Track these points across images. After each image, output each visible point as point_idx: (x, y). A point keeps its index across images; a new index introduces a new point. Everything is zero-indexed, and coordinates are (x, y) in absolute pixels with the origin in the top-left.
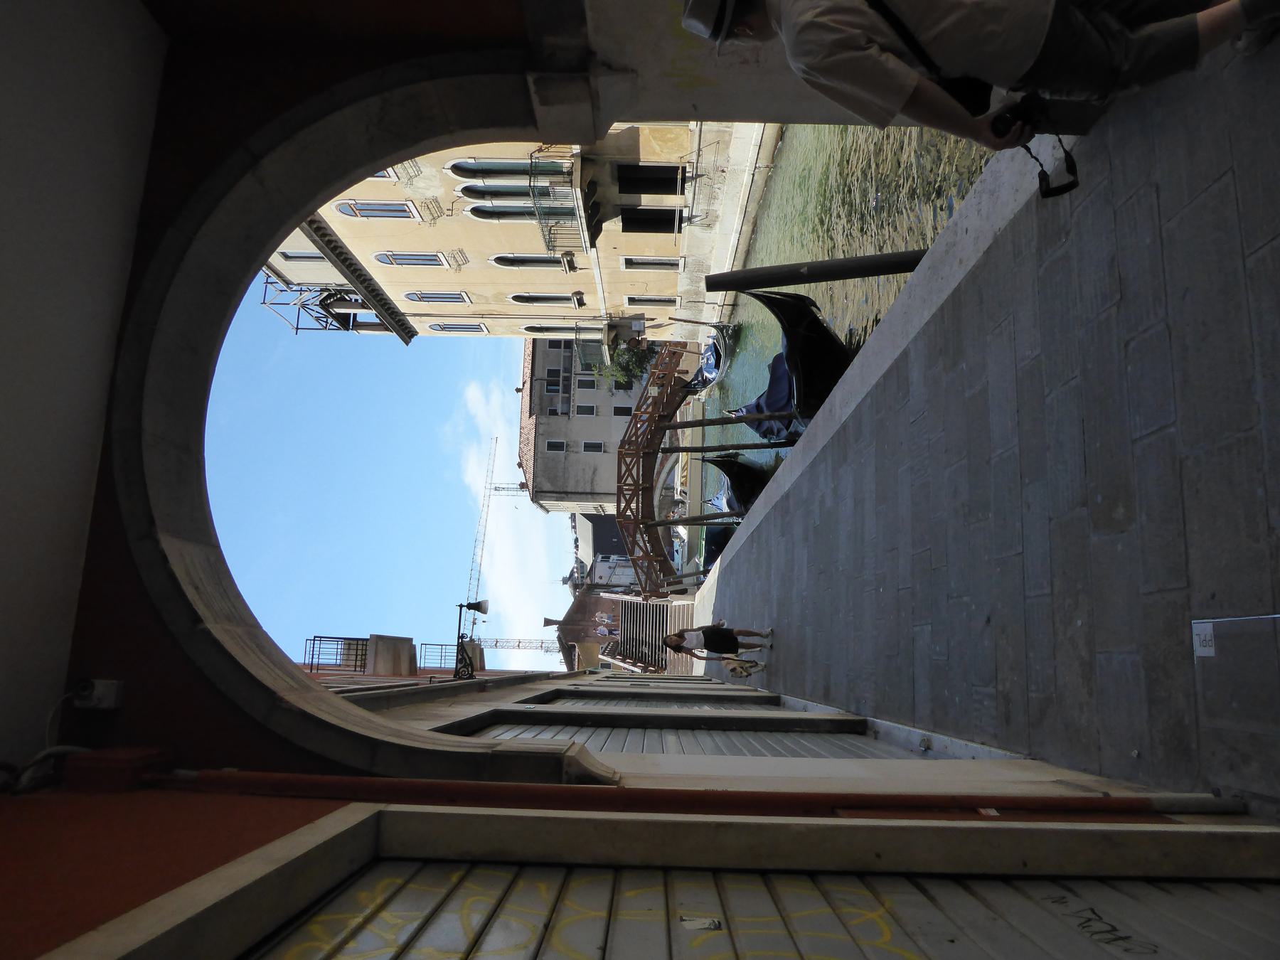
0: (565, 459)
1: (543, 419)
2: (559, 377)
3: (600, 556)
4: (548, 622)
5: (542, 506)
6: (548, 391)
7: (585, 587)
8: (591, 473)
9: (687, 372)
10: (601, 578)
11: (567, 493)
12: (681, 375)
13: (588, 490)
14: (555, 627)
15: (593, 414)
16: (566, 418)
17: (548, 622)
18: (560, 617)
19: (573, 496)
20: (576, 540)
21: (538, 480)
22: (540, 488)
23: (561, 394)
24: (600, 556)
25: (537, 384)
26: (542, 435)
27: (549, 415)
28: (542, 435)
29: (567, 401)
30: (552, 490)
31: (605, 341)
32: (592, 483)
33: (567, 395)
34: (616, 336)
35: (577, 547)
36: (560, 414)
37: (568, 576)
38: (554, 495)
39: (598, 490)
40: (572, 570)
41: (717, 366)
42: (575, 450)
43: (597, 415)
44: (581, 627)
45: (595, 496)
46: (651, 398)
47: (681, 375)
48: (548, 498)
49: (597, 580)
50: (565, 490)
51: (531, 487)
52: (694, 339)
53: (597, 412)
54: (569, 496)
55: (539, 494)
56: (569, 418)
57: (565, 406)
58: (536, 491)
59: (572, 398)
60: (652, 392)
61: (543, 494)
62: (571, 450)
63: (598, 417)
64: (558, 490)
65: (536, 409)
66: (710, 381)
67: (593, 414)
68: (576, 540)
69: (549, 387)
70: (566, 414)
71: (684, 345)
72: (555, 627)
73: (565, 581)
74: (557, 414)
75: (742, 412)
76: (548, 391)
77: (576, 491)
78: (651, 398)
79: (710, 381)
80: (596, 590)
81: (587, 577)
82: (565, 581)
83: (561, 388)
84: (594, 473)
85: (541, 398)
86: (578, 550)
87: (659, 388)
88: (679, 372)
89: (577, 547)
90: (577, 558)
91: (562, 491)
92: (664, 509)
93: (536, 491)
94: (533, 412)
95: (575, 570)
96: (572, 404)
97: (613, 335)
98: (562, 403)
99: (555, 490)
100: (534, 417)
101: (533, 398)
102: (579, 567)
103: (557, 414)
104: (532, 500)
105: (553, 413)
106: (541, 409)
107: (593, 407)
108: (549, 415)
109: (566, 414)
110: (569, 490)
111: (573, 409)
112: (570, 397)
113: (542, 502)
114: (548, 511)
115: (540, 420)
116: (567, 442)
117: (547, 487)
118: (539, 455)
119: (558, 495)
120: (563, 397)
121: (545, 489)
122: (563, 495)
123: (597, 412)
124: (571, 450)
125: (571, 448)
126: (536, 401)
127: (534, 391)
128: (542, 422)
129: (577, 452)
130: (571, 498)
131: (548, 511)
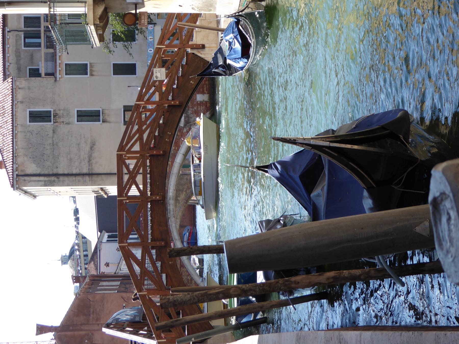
0: (54, 132)
1: (23, 83)
2: (40, 27)
3: (106, 235)
4: (41, 329)
5: (26, 192)
6: (26, 45)
7: (87, 280)
8: (88, 148)
9: (203, 47)
10: (107, 265)
11: (57, 175)
12: (195, 52)
13: (85, 171)
14: (50, 335)
15: (87, 75)
16: (51, 79)
17: (41, 329)
18: (57, 322)
19: (66, 178)
20: (76, 212)
21: (19, 160)
22: (22, 171)
23: (43, 50)
24: (106, 235)
25: (11, 37)
26: (22, 102)
27: (30, 77)
28: (22, 102)
29: (53, 58)
30: (38, 172)
31: (90, 18)
32: (89, 161)
33: (51, 51)
34: (106, 11)
35: (77, 219)
36: (43, 75)
37: (68, 254)
38: (42, 178)
39: (96, 171)
40: (73, 247)
41: (245, 54)
42: (65, 120)
43: (92, 75)
44: (83, 333)
45: (95, 178)
46: (158, 82)
47: (195, 52)
48: (33, 183)
49: (104, 269)
50: (55, 171)
51: (9, 164)
52: (210, 10)
53: (91, 71)
54: (61, 178)
55: (20, 177)
56: (56, 80)
57: (50, 64)
58: (17, 175)
59: (58, 54)
60: (158, 75)
61: (26, 178)
62: (61, 120)
63: (93, 78)
64: (46, 172)
65: (12, 69)
66: (236, 70)
67: (87, 75)
68: (76, 212)
69: (28, 40)
70: (52, 74)
71: (194, 17)
72: (50, 335)
73: (64, 261)
74: (39, 75)
75: (277, 169)
76: (26, 45)
77: (70, 172)
78: (158, 82)
79: (236, 70)
80: (101, 283)
81: (90, 262)
82: (64, 261)
83: (42, 41)
84: (91, 148)
85: (18, 53)
86: (78, 223)
87: (166, 70)
88: (193, 47)
89: (77, 219)
90: (77, 233)
91: (51, 173)
92: (182, 191)
93: (17, 175)
94: (7, 73)
95: (76, 247)
96: (58, 61)
97: (100, 10)
98: (46, 60)
99: (42, 173)
100: (10, 80)
101: (7, 55)
102: (81, 245)
103: (39, 75)
104: (13, 186)
105: (35, 73)
106: (19, 69)
107: (87, 64)
108: (30, 77)
109: (52, 74)
110: (61, 172)
111: (61, 69)
112: (56, 52)
113: (25, 188)
114: (35, 197)
115: (18, 83)
116: (55, 111)
117: (31, 168)
118: (20, 129)
119: (46, 179)
120: (46, 54)
121: (29, 171)
122: (53, 178)
123: (91, 71)
124: (61, 120)
125: (59, 117)
126: (10, 59)
127: (7, 46)
128: (20, 86)
129: (68, 124)
130: (63, 181)
131: (35, 197)
